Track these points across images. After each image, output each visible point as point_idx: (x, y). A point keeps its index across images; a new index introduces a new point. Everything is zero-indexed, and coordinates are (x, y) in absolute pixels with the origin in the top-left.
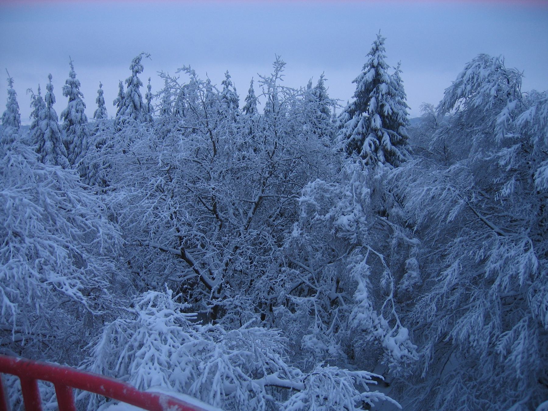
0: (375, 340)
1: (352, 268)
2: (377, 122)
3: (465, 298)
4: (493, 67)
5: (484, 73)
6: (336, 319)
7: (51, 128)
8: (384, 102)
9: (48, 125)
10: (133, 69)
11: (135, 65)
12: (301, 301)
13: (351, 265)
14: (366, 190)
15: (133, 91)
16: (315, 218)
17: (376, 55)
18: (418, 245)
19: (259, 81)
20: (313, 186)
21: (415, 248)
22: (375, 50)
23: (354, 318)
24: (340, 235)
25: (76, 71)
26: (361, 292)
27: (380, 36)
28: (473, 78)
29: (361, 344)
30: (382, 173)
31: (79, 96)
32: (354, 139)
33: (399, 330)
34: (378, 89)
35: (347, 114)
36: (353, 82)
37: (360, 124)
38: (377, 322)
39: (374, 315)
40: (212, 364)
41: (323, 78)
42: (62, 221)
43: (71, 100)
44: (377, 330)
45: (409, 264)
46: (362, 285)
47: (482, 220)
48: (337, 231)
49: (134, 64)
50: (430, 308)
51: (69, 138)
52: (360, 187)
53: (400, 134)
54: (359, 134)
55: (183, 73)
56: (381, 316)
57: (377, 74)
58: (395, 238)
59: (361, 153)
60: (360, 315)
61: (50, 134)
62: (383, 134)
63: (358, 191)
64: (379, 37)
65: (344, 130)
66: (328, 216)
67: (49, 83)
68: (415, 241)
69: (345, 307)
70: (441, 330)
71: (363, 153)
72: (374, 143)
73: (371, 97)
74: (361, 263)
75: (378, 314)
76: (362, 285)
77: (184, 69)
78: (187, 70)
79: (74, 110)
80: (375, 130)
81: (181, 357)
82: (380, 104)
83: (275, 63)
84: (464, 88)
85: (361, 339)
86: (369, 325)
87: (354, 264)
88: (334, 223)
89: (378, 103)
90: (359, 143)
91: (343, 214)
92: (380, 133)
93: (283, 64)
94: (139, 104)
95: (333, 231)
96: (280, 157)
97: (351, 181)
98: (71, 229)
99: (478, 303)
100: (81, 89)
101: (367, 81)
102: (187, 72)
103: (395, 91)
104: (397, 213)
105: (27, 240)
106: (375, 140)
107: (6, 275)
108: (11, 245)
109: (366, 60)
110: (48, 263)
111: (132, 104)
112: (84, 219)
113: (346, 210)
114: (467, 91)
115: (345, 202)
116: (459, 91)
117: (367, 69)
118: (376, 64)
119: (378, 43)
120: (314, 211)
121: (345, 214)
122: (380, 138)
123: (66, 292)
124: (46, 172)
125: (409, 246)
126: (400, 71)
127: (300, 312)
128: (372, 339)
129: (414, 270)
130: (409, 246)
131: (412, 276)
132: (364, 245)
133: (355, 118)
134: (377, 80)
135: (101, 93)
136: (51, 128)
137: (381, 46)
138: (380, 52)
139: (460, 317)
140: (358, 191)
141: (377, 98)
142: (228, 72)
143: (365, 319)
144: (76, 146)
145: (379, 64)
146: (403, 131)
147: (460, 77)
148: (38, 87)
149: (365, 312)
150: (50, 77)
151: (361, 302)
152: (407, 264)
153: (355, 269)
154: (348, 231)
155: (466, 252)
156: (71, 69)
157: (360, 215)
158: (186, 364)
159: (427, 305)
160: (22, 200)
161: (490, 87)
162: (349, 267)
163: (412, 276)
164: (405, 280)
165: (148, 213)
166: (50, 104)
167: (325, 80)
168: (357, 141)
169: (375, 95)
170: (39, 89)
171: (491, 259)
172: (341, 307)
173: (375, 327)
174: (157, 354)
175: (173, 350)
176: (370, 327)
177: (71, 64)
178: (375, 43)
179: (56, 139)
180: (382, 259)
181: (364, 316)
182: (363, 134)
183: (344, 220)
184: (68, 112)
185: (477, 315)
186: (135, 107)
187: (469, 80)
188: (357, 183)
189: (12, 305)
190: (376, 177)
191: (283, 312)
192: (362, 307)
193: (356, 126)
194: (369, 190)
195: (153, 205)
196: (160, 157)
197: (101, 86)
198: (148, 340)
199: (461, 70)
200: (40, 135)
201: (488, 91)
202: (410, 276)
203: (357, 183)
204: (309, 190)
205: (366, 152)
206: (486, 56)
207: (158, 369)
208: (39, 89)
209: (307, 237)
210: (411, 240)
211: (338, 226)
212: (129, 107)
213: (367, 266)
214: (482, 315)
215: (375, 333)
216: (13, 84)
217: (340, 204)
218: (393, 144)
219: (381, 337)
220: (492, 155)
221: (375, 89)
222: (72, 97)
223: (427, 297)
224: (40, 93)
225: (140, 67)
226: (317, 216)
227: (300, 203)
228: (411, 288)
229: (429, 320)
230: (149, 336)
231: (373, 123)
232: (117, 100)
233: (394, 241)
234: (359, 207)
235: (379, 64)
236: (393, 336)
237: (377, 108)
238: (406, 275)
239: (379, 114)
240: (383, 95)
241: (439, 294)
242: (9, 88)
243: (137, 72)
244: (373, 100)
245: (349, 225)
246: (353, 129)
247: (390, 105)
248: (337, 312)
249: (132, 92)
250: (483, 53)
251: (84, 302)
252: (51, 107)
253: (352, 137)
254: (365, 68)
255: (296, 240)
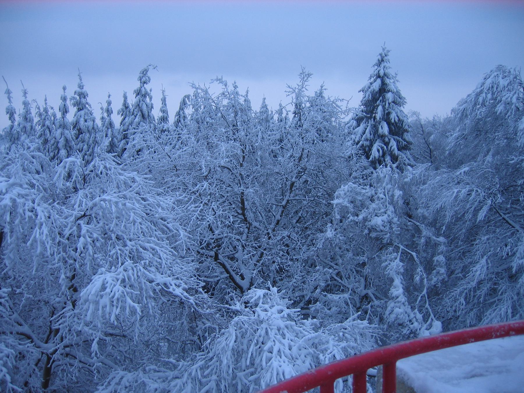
0: (410, 333)
1: (387, 266)
2: (384, 129)
3: (493, 291)
4: (512, 77)
5: (503, 83)
6: (370, 314)
7: (65, 137)
8: (390, 110)
9: (62, 134)
10: (141, 80)
11: (143, 77)
12: (338, 298)
13: (386, 263)
14: (398, 193)
15: (141, 101)
16: (349, 220)
17: (382, 65)
18: (444, 243)
19: (286, 91)
20: (346, 190)
21: (442, 246)
22: (381, 61)
23: (390, 313)
24: (373, 235)
25: (84, 82)
26: (397, 289)
27: (385, 48)
28: (492, 87)
29: (397, 337)
30: (411, 176)
31: (87, 106)
32: (363, 145)
33: (433, 323)
34: (384, 97)
35: (355, 122)
36: (359, 92)
37: (367, 131)
38: (412, 315)
39: (409, 310)
40: (330, 355)
41: (323, 88)
42: (147, 225)
43: (79, 110)
44: (412, 324)
45: (437, 261)
46: (397, 282)
47: (504, 219)
48: (370, 231)
49: (141, 75)
50: (459, 302)
51: (78, 146)
52: (391, 189)
53: (405, 140)
54: (367, 140)
55: (216, 83)
56: (416, 311)
57: (383, 83)
58: (424, 237)
59: (371, 159)
60: (397, 310)
61: (65, 143)
62: (389, 140)
63: (390, 193)
64: (384, 49)
65: (353, 136)
66: (361, 217)
67: (63, 93)
68: (441, 239)
69: (376, 302)
70: (470, 323)
71: (373, 158)
72: (382, 148)
73: (378, 106)
74: (396, 261)
75: (413, 308)
76: (397, 282)
77: (217, 80)
78: (220, 81)
79: (82, 120)
80: (382, 137)
81: (300, 350)
82: (386, 112)
83: (301, 74)
84: (485, 97)
85: (397, 332)
86: (404, 318)
87: (389, 262)
88: (366, 224)
89: (384, 111)
90: (367, 149)
91: (376, 216)
92: (387, 140)
93: (309, 75)
94: (147, 114)
95: (366, 231)
96: (311, 164)
97: (384, 185)
98: (155, 232)
99: (505, 296)
100: (89, 100)
101: (374, 90)
102: (220, 83)
103: (400, 100)
104: (423, 213)
105: (129, 243)
106: (383, 145)
107: (124, 276)
108: (118, 248)
109: (372, 71)
110: (151, 264)
111: (140, 113)
112: (166, 222)
113: (380, 212)
114: (488, 99)
115: (378, 204)
116: (481, 100)
117: (372, 79)
118: (382, 74)
119: (383, 55)
120: (348, 212)
121: (379, 215)
122: (387, 144)
123: (174, 292)
124: (125, 178)
125: (436, 245)
126: (398, 81)
127: (336, 308)
128: (408, 332)
129: (441, 267)
130: (436, 244)
131: (440, 272)
132: (396, 244)
133: (362, 126)
134: (383, 90)
135: (109, 103)
136: (65, 137)
137: (386, 58)
138: (385, 63)
139: (487, 310)
140: (390, 193)
141: (384, 107)
142: (235, 83)
143: (402, 313)
144: (86, 154)
145: (385, 74)
146: (408, 137)
147: (480, 86)
148: (44, 98)
149: (401, 307)
150: (64, 89)
151: (398, 297)
152: (435, 261)
153: (390, 267)
154: (382, 231)
155: (492, 249)
156: (79, 80)
157: (393, 216)
158: (305, 356)
159: (455, 300)
160: (125, 205)
161: (511, 96)
162: (384, 264)
163: (440, 272)
164: (433, 277)
165: (195, 216)
166: (64, 114)
167: (325, 89)
168: (366, 147)
169: (381, 103)
170: (46, 100)
171: (518, 255)
172: (373, 304)
173: (410, 321)
174: (282, 348)
175: (292, 343)
176: (406, 321)
177: (79, 75)
178: (381, 55)
179: (70, 147)
180: (415, 256)
181: (401, 310)
182: (371, 140)
183: (378, 221)
184: (77, 121)
185: (506, 307)
186: (143, 116)
187: (489, 89)
188: (389, 186)
189: (136, 305)
190: (406, 180)
191: (319, 309)
192: (399, 302)
193: (364, 133)
194: (401, 192)
195: (199, 209)
196: (203, 163)
197: (109, 96)
198: (272, 334)
199: (481, 80)
200: (54, 143)
201: (509, 99)
202: (438, 273)
203: (389, 186)
204: (342, 193)
205: (375, 157)
206: (503, 66)
207: (287, 362)
208: (46, 100)
209: (341, 238)
210: (437, 239)
211: (372, 226)
212: (138, 116)
213: (401, 264)
214: (510, 307)
215: (411, 326)
216: (27, 95)
217: (374, 205)
218: (399, 150)
219: (416, 330)
220: (516, 159)
221: (381, 98)
222: (80, 107)
223: (456, 292)
224: (46, 104)
225: (147, 78)
226: (351, 218)
227: (334, 206)
228: (440, 284)
229: (458, 314)
230: (271, 331)
231: (380, 130)
232: (121, 110)
233: (423, 240)
234: (391, 208)
235: (385, 74)
236: (427, 329)
237: (384, 115)
238: (434, 271)
239: (385, 121)
240: (389, 104)
241: (466, 289)
242: (23, 99)
243: (145, 83)
244: (380, 108)
245: (383, 226)
246: (362, 136)
247: (396, 113)
248: (370, 308)
249: (140, 102)
250: (500, 64)
251: (191, 301)
252: (65, 116)
253: (361, 143)
254: (371, 78)
255: (329, 241)
